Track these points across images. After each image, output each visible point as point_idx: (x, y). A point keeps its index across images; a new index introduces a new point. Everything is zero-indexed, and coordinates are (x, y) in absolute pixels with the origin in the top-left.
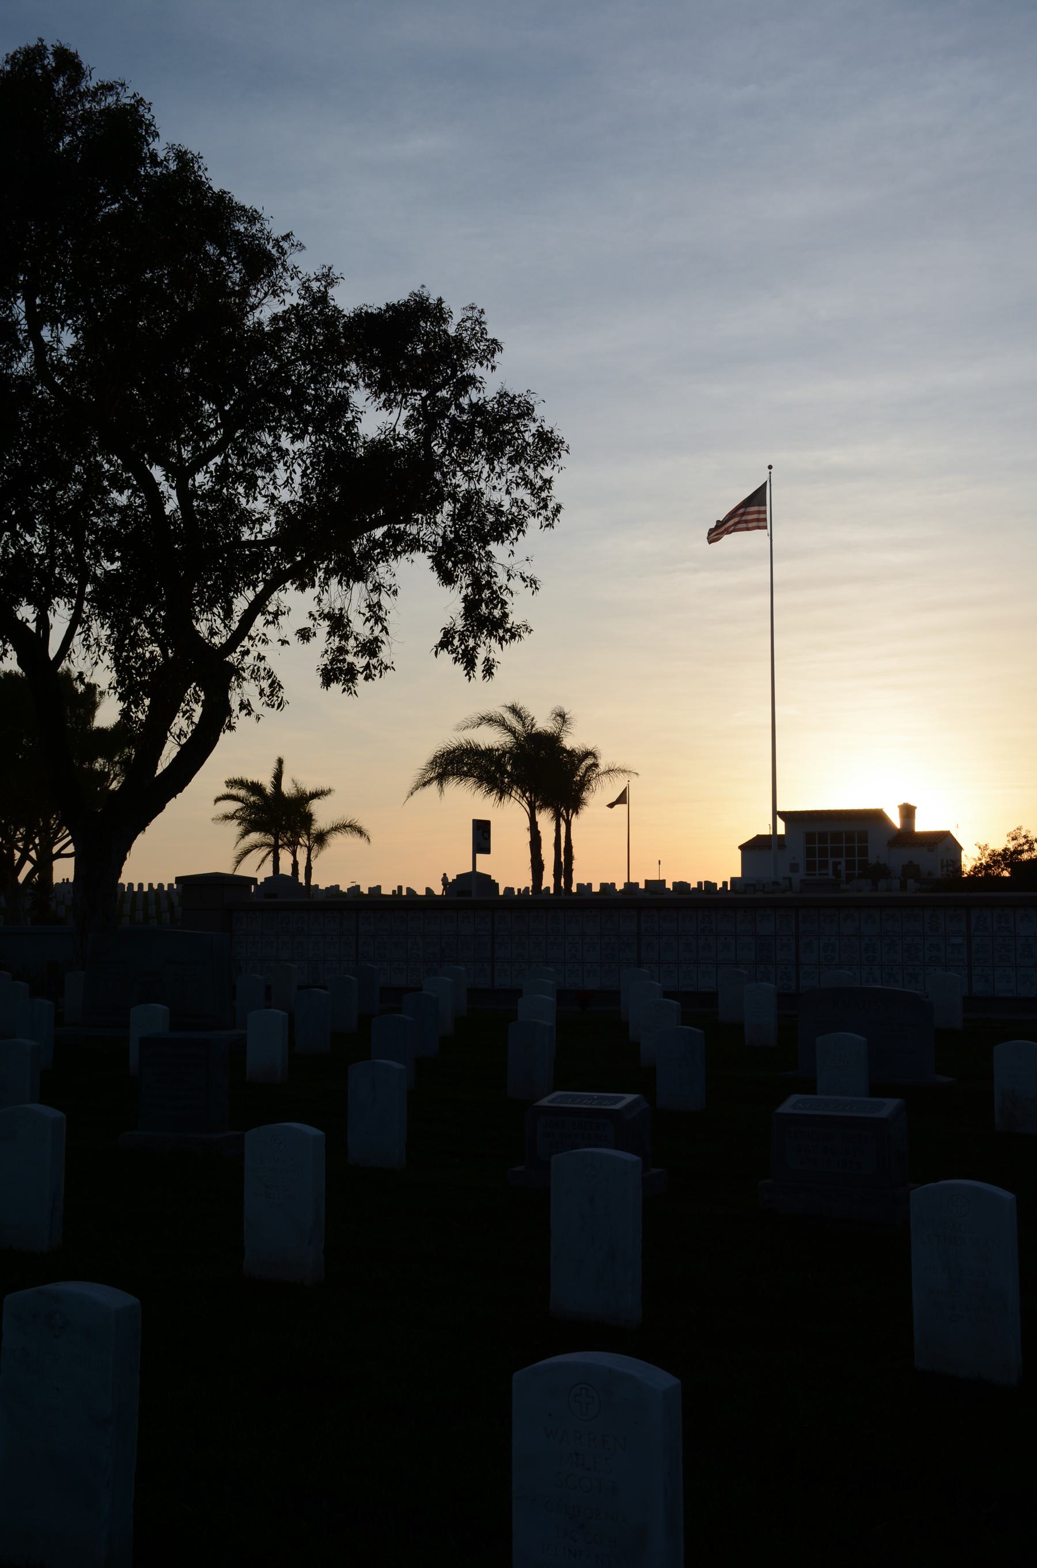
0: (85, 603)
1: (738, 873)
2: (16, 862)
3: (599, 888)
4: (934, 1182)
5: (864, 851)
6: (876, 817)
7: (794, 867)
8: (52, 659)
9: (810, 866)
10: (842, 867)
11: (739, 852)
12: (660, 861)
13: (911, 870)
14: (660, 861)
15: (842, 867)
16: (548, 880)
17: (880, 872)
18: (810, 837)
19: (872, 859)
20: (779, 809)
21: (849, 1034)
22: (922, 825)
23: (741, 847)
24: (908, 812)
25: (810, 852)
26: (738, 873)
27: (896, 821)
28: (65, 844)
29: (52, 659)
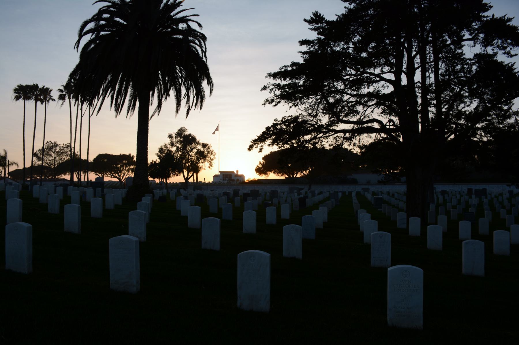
0: (440, 63)
1: (213, 180)
2: (167, 80)
3: (27, 167)
4: (116, 95)
5: (231, 177)
6: (233, 172)
7: (221, 179)
8: (402, 73)
9: (223, 179)
10: (228, 179)
11: (213, 177)
12: (205, 179)
13: (238, 180)
14: (205, 179)
15: (228, 179)
16: (195, 181)
17: (233, 180)
18: (223, 175)
19: (232, 178)
20: (220, 171)
21: (241, 253)
22: (239, 173)
23: (213, 176)
24: (237, 171)
25: (223, 177)
26: (213, 180)
27: (236, 173)
28: (462, 116)
29: (402, 73)
